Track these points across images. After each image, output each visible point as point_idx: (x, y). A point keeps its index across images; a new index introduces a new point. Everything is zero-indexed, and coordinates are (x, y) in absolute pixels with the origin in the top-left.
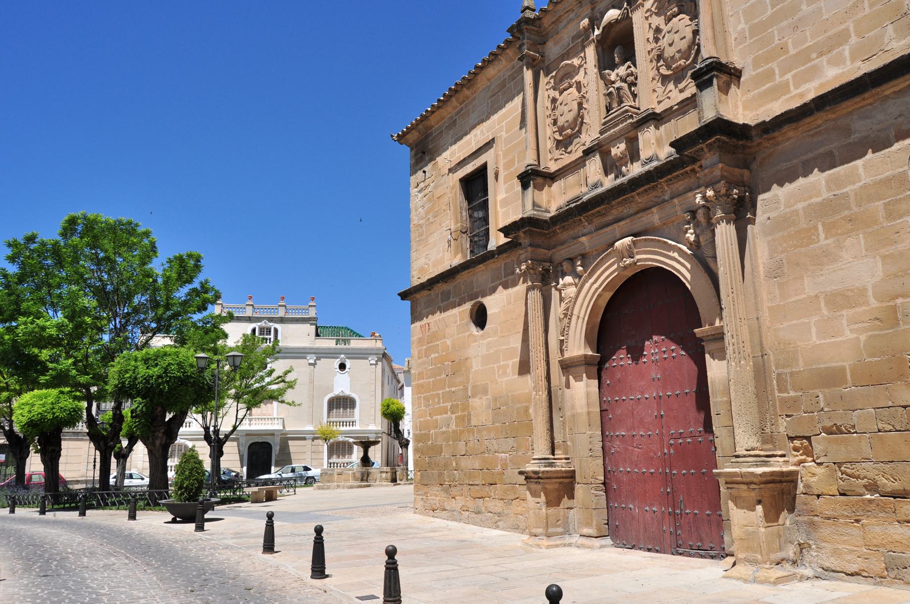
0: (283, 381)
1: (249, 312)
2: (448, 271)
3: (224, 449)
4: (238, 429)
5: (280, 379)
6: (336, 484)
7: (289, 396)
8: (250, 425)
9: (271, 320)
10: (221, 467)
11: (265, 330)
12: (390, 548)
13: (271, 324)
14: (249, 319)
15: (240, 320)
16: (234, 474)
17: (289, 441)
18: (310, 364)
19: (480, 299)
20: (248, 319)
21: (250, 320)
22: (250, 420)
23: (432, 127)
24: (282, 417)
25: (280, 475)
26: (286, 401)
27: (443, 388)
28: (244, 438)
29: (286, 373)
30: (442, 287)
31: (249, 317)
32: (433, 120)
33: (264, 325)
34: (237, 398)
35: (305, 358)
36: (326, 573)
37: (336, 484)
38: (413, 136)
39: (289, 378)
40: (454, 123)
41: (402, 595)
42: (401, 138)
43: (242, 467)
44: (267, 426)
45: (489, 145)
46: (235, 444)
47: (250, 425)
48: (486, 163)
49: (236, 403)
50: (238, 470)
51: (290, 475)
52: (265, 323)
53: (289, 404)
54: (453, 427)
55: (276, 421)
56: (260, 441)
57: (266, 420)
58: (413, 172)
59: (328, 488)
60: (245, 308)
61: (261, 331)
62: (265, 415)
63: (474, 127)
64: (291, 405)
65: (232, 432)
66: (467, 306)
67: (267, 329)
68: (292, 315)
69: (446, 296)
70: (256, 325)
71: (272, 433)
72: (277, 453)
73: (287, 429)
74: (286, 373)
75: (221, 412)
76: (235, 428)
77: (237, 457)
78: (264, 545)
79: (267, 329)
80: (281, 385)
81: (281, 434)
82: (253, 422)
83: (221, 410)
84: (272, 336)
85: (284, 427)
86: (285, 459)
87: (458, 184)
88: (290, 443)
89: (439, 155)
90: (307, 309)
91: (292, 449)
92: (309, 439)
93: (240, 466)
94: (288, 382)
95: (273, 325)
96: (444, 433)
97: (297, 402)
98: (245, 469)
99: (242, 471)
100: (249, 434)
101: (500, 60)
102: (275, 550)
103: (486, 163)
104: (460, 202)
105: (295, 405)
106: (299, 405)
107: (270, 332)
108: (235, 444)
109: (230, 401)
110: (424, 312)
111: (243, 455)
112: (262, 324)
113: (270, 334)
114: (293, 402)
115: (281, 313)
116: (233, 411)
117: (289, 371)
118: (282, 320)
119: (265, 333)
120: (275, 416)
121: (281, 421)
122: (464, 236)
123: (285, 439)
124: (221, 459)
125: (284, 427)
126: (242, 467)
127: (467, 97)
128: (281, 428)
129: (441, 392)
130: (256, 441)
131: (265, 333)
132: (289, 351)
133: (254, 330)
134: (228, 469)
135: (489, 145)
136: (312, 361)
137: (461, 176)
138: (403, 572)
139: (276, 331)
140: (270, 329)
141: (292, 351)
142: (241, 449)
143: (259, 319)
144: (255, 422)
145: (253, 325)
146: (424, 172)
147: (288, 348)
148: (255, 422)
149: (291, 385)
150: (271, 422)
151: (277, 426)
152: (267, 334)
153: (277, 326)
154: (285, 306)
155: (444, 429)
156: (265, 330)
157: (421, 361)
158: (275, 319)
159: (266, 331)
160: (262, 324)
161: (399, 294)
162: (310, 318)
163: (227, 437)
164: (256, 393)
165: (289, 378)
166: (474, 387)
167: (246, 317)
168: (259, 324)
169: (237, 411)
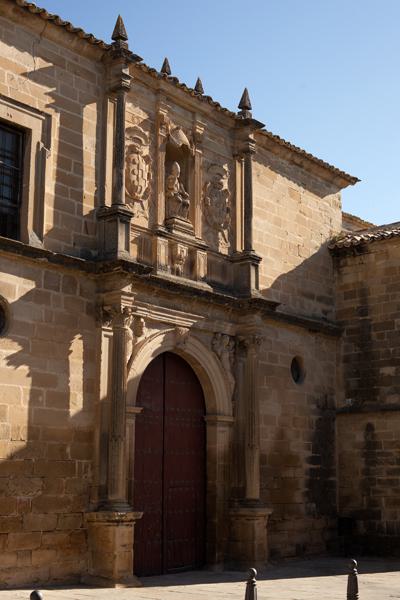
101: (73, 39)
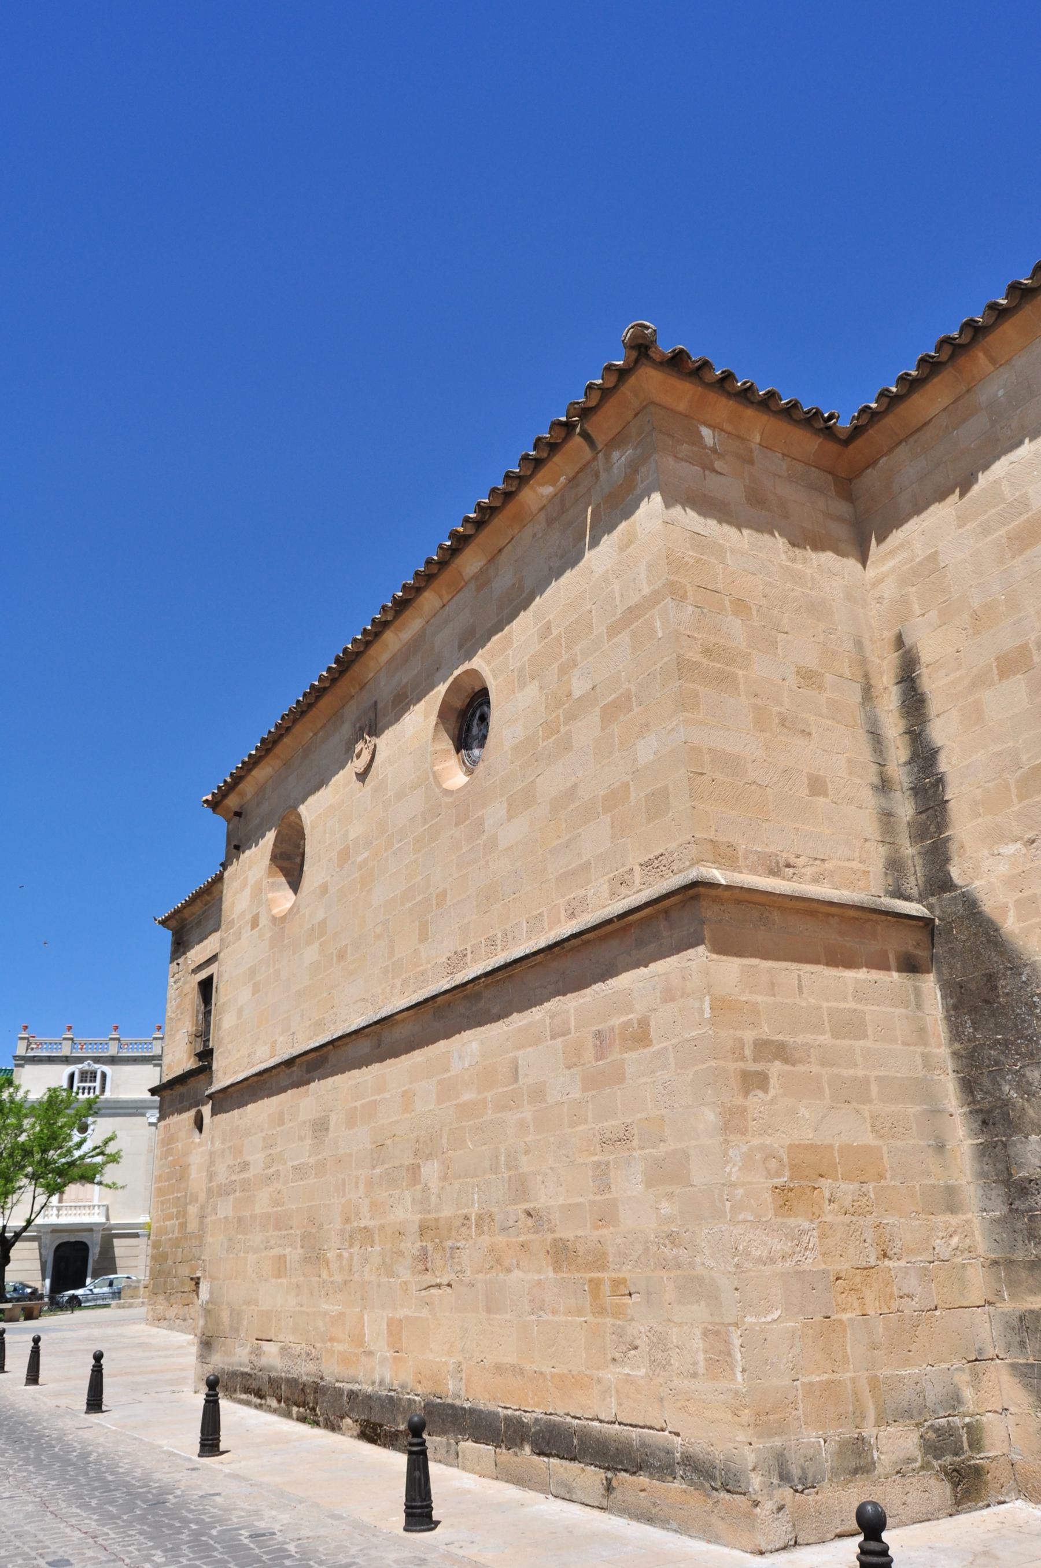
0: (102, 1153)
1: (66, 1050)
2: (180, 1076)
3: (13, 1253)
4: (33, 1224)
5: (98, 1150)
6: (141, 1300)
7: (110, 1173)
8: (58, 1216)
9: (97, 1060)
10: (6, 1279)
11: (89, 1075)
12: (211, 1377)
13: (97, 1066)
14: (66, 1060)
15: (53, 1061)
16: (29, 1290)
17: (115, 1240)
18: (151, 1124)
19: (200, 1107)
20: (64, 1059)
21: (67, 1061)
22: (59, 1209)
23: (186, 919)
24: (105, 1203)
25: (91, 1290)
26: (105, 1182)
27: (173, 1194)
28: (49, 1236)
29: (106, 1143)
30: (180, 1089)
31: (67, 1057)
32: (187, 913)
33: (87, 1068)
34: (34, 1177)
35: (143, 1115)
36: (221, 1449)
37: (141, 1300)
38: (173, 923)
39: (110, 1149)
40: (200, 921)
41: (221, 1433)
42: (163, 923)
43: (44, 1279)
44: (83, 1217)
45: (214, 959)
46: (36, 1244)
47: (58, 1216)
48: (212, 975)
49: (33, 1187)
50: (38, 1285)
51: (106, 1289)
52: (89, 1064)
53: (107, 1186)
54: (176, 1234)
55: (96, 1210)
56: (73, 1240)
57: (96, 1208)
58: (172, 961)
59: (130, 1306)
60: (60, 1044)
61: (82, 1077)
62: (81, 1200)
63: (210, 934)
64: (110, 1188)
65: (25, 1229)
66: (192, 1113)
67: (91, 1073)
68: (133, 1052)
69: (182, 1098)
70: (76, 1068)
71: (89, 1228)
72: (96, 1257)
73: (112, 1222)
74: (106, 1143)
75: (9, 1200)
76: (29, 1222)
77: (37, 1265)
78: (88, 1400)
79: (91, 1073)
80: (99, 1159)
81: (104, 1230)
82: (63, 1212)
83: (10, 1197)
84: (97, 1084)
85: (108, 1219)
86: (108, 1265)
87: (197, 986)
88: (116, 1242)
89: (189, 951)
90: (150, 1044)
91: (117, 1252)
92: (144, 1235)
93: (40, 1278)
94: (108, 1155)
95: (100, 1068)
96: (170, 1239)
97: (120, 1184)
98: (48, 1282)
99: (43, 1286)
100: (56, 1230)
102: (222, 1447)
103: (212, 975)
104: (197, 1006)
105: (117, 1188)
106: (123, 1187)
107: (95, 1077)
108: (36, 1244)
109: (24, 1181)
110: (168, 1111)
111: (46, 1261)
112: (84, 1066)
113: (95, 1081)
114: (114, 1184)
115: (113, 1050)
116: (27, 1196)
117: (111, 1139)
118: (113, 1060)
119: (88, 1079)
120: (96, 1202)
121: (103, 1210)
122: (199, 1040)
123: (108, 1236)
124: (7, 1268)
125: (108, 1219)
126: (44, 1279)
127: (209, 902)
128: (103, 1220)
129: (171, 1197)
130: (66, 1240)
131: (88, 1079)
132: (119, 1105)
133: (72, 1076)
134: (21, 1284)
135: (214, 959)
136: (154, 1120)
137: (200, 979)
138: (43, 1360)
139: (104, 1076)
140: (96, 1073)
141: (125, 1105)
142: (44, 1252)
143: (80, 1060)
144: (65, 1212)
145: (69, 1069)
146: (178, 964)
147: (119, 1102)
148: (65, 1212)
149: (114, 1159)
150: (88, 1212)
151: (96, 1217)
152: (91, 1081)
153: (106, 1068)
154: (118, 1039)
155: (171, 1236)
156: (89, 1075)
157: (162, 1162)
158: (101, 1059)
159: (88, 1076)
160: (84, 1066)
161: (150, 1090)
162: (153, 1056)
163: (17, 1236)
164: (60, 1172)
165: (110, 1149)
166: (191, 1194)
167: (62, 1057)
168: (80, 1066)
169: (34, 1198)
